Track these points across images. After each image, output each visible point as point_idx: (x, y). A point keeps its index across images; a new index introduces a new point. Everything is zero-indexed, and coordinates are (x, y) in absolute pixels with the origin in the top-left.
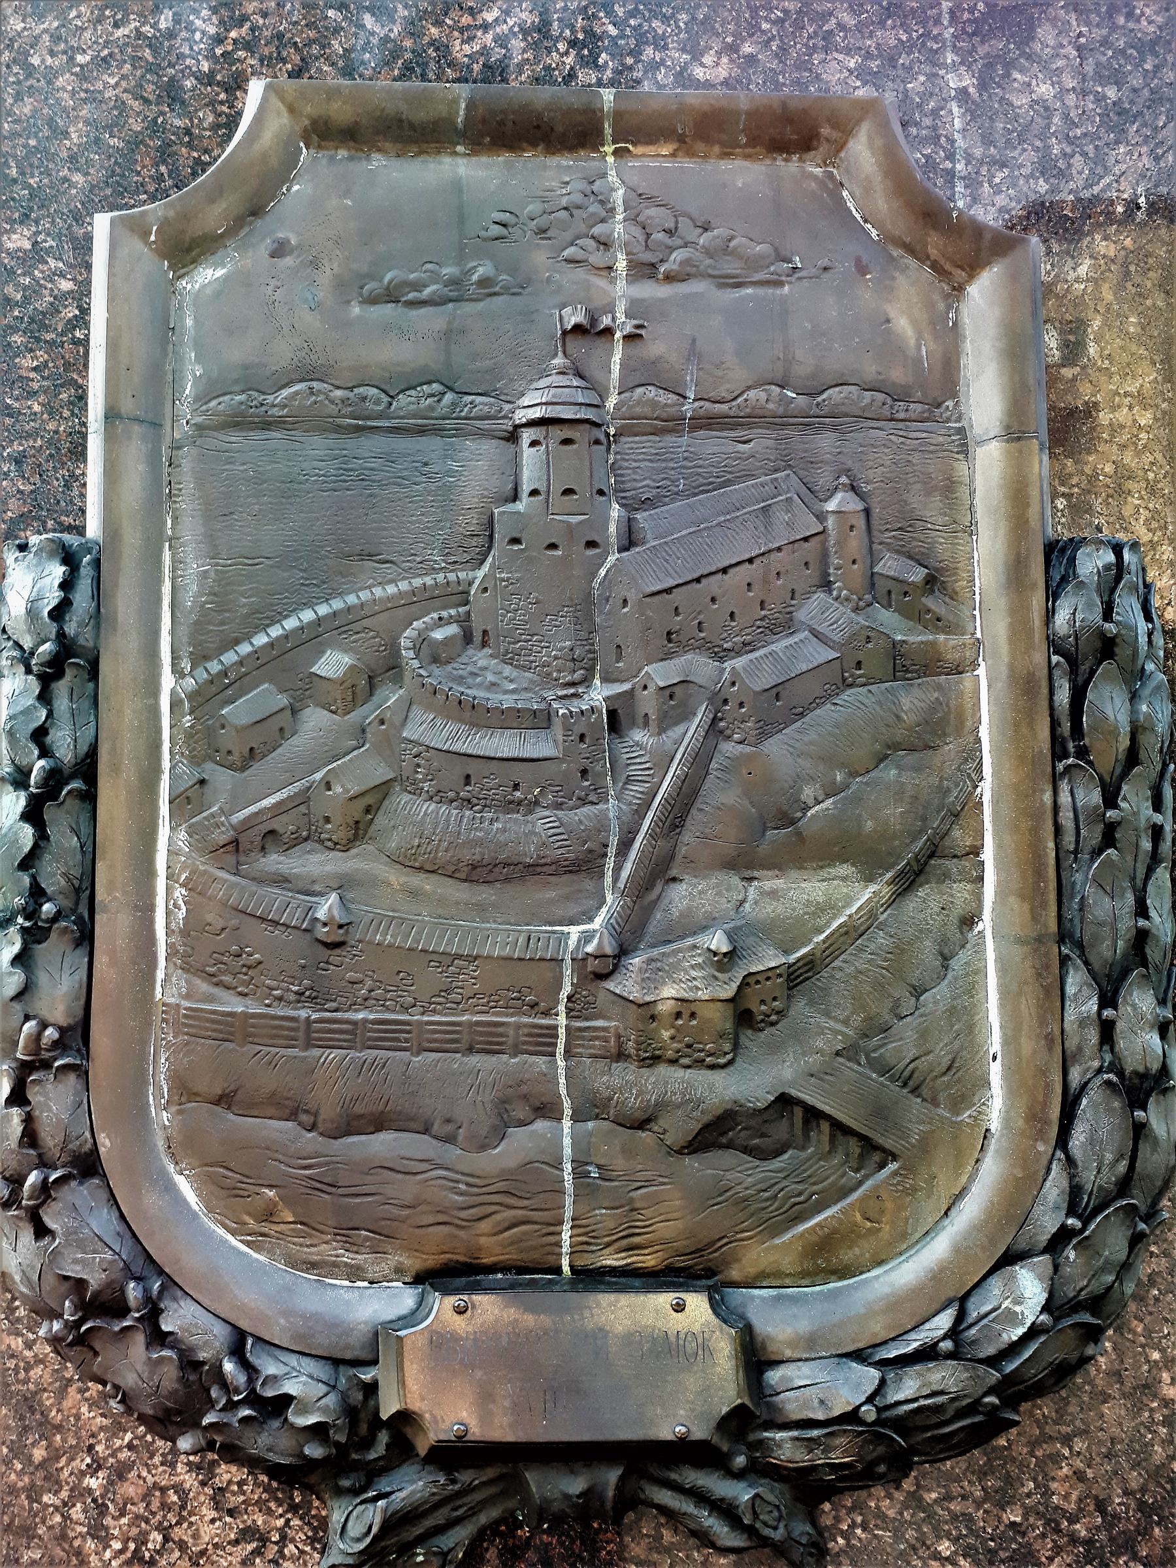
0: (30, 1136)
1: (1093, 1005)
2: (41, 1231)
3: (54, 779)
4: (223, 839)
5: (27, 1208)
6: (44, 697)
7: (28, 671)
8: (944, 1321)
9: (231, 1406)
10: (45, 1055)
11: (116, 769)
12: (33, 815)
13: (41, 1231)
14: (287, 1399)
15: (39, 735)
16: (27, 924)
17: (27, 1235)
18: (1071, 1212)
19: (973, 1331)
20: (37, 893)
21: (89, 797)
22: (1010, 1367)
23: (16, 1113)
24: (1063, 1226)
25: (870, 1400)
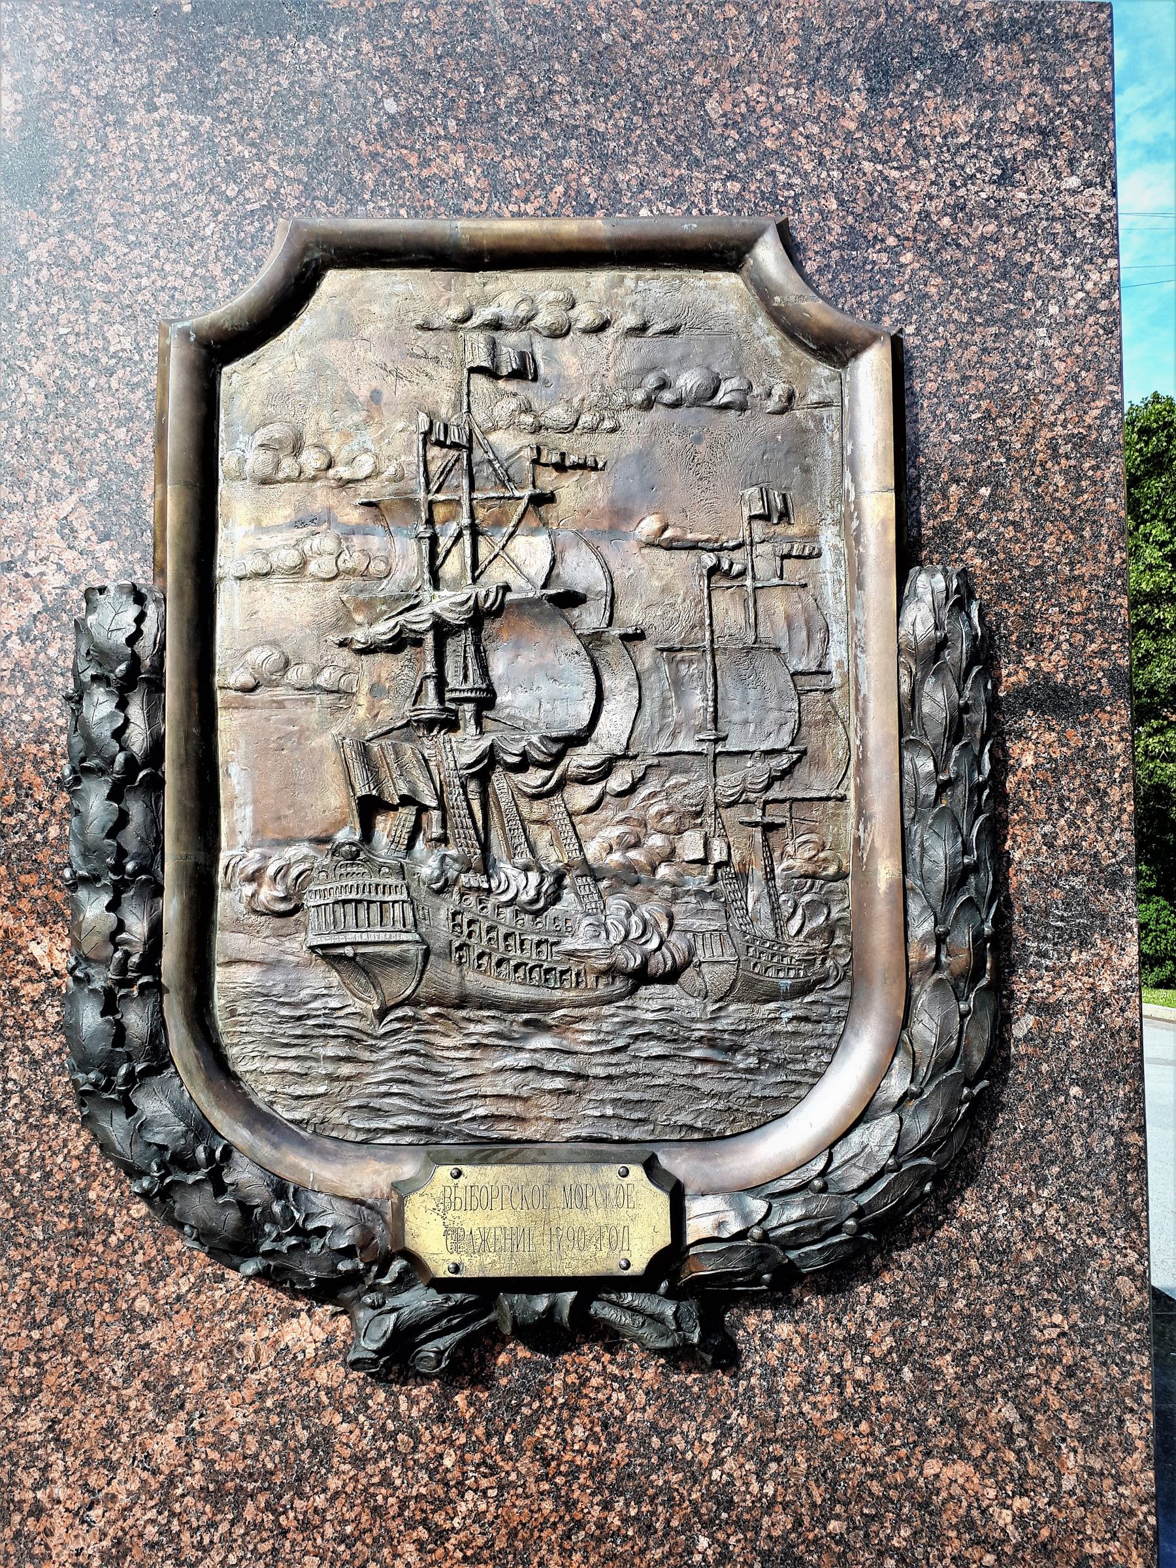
6: (122, 705)
12: (115, 795)
22: (865, 1198)
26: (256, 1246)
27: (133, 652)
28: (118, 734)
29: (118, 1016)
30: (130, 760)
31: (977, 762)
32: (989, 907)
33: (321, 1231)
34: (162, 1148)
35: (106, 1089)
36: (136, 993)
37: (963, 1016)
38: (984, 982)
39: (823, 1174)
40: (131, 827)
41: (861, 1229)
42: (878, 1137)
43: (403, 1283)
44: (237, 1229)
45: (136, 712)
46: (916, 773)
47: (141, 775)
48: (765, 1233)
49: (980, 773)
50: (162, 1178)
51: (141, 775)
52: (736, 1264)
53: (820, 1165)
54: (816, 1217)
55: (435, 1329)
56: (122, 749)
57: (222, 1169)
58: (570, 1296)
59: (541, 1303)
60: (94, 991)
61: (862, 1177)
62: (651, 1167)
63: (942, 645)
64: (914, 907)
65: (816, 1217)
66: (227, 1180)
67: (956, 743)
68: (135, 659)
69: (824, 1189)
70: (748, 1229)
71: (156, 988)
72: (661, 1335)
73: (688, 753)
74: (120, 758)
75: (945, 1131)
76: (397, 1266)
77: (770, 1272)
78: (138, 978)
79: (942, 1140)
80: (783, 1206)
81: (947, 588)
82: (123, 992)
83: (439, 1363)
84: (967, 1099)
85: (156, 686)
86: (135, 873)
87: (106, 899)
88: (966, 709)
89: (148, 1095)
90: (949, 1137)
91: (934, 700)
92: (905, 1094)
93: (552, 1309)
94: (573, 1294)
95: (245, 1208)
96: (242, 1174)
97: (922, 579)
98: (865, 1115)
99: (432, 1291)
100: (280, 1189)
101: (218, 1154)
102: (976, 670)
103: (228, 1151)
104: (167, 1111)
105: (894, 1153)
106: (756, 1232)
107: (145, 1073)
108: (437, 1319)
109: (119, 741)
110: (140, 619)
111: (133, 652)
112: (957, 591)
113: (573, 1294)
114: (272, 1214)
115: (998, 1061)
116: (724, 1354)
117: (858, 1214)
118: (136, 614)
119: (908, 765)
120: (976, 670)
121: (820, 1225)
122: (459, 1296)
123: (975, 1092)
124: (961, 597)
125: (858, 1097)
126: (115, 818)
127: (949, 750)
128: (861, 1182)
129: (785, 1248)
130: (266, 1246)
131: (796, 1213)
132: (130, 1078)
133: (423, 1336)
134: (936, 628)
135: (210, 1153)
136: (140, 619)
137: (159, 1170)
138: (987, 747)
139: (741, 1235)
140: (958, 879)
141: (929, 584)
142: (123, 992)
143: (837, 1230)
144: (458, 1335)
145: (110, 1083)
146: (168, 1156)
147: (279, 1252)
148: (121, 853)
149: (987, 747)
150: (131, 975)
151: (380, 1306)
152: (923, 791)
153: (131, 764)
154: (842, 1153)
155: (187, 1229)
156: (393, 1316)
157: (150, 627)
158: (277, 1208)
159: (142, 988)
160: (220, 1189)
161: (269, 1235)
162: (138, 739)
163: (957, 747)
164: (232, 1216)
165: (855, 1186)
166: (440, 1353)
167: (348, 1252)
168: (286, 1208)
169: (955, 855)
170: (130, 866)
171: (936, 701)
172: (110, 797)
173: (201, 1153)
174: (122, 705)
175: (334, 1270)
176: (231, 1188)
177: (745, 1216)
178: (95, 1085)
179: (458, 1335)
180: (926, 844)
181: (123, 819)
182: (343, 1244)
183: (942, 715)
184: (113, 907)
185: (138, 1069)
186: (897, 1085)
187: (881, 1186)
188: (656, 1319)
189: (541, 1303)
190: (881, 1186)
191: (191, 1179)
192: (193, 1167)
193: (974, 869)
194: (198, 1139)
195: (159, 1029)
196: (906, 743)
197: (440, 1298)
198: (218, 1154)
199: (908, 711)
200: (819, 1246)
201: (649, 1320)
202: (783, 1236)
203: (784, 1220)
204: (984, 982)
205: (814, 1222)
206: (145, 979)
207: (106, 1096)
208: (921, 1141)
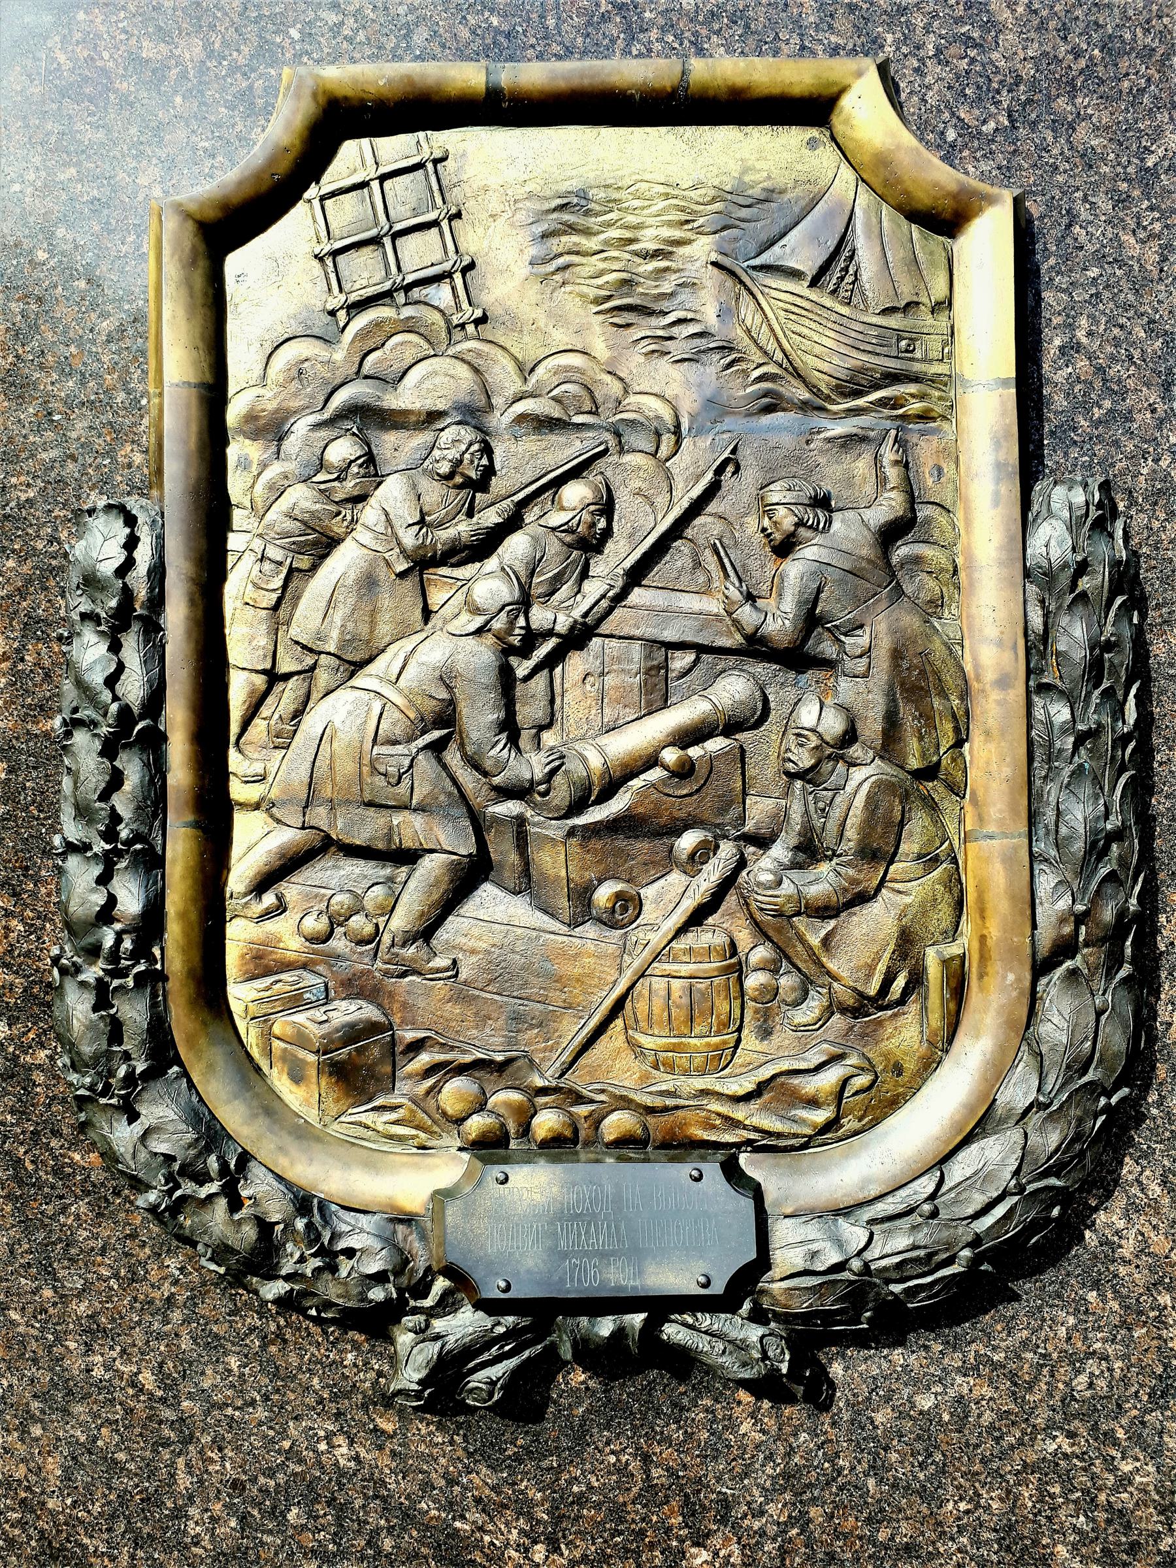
6: (115, 647)
12: (109, 750)
26: (277, 1266)
27: (125, 584)
28: (111, 681)
29: (113, 1011)
30: (125, 711)
31: (1118, 713)
32: (1135, 881)
33: (350, 1253)
34: (169, 1159)
35: (103, 1094)
36: (131, 984)
37: (1099, 1013)
38: (1122, 973)
39: (932, 1197)
40: (127, 787)
41: (975, 1261)
42: (995, 1154)
43: (447, 1305)
44: (253, 1250)
45: (132, 652)
46: (1049, 724)
48: (866, 1265)
49: (1124, 722)
50: (170, 1193)
52: (829, 1304)
53: (927, 1185)
55: (485, 1357)
56: (115, 698)
58: (637, 1319)
59: (605, 1327)
60: (83, 984)
61: (979, 1200)
62: (732, 1172)
63: (1082, 568)
64: (1046, 882)
65: (925, 1247)
66: (244, 1193)
67: (1096, 687)
68: (127, 594)
69: (934, 1214)
70: (847, 1261)
71: (153, 980)
72: (744, 1365)
74: (114, 708)
75: (1078, 1147)
76: (441, 1284)
77: (867, 1310)
78: (133, 966)
79: (1072, 1158)
80: (888, 1233)
81: (1087, 503)
82: (116, 983)
83: (491, 1394)
84: (1102, 1112)
85: (152, 628)
86: (129, 843)
87: (97, 870)
88: (1109, 646)
90: (1082, 1153)
91: (1070, 636)
92: (1031, 1106)
93: (620, 1333)
94: (643, 1316)
95: (264, 1227)
96: (258, 1186)
97: (1059, 493)
98: (981, 1123)
99: (480, 1314)
100: (303, 1202)
101: (232, 1166)
102: (1119, 600)
103: (245, 1158)
104: (173, 1116)
105: (1017, 1173)
106: (856, 1264)
107: (148, 1076)
108: (487, 1346)
109: (113, 691)
110: (131, 543)
111: (125, 584)
112: (1100, 506)
113: (643, 1316)
114: (294, 1231)
115: (1139, 1062)
116: (818, 1393)
117: (976, 1242)
118: (122, 540)
119: (1039, 713)
120: (1119, 600)
121: (930, 1256)
122: (510, 1320)
123: (1114, 1100)
124: (1102, 518)
125: (971, 1108)
126: (107, 778)
127: (1089, 694)
128: (979, 1207)
129: (888, 1281)
130: (287, 1268)
131: (901, 1242)
133: (471, 1365)
134: (1074, 549)
135: (224, 1165)
136: (131, 543)
138: (1133, 691)
139: (839, 1267)
140: (1097, 849)
141: (1065, 498)
142: (116, 983)
143: (950, 1261)
144: (513, 1362)
145: (107, 1088)
146: (176, 1167)
147: (303, 1276)
148: (115, 818)
149: (1133, 691)
150: (125, 963)
151: (423, 1331)
152: (1058, 744)
153: (126, 716)
154: (958, 1171)
155: (200, 1247)
156: (439, 1344)
157: (144, 555)
158: (300, 1224)
159: (137, 977)
160: (235, 1204)
162: (133, 688)
163: (1097, 693)
164: (250, 1232)
165: (970, 1211)
166: (493, 1383)
167: (380, 1278)
168: (309, 1226)
170: (124, 834)
171: (1074, 635)
172: (102, 754)
173: (213, 1163)
174: (115, 647)
175: (363, 1298)
176: (248, 1203)
177: (839, 1243)
178: (91, 1088)
179: (513, 1362)
180: (1062, 807)
181: (116, 781)
183: (1079, 654)
184: (104, 880)
186: (1018, 1092)
187: (1000, 1211)
188: (740, 1346)
189: (605, 1327)
190: (1000, 1211)
191: (203, 1192)
192: (202, 1178)
193: (1117, 835)
194: (208, 1150)
196: (1037, 688)
197: (488, 1322)
198: (232, 1166)
199: (1037, 646)
200: (929, 1279)
201: (730, 1347)
202: (885, 1269)
203: (888, 1250)
204: (1122, 973)
205: (922, 1253)
206: (141, 967)
207: (103, 1101)
208: (1049, 1159)
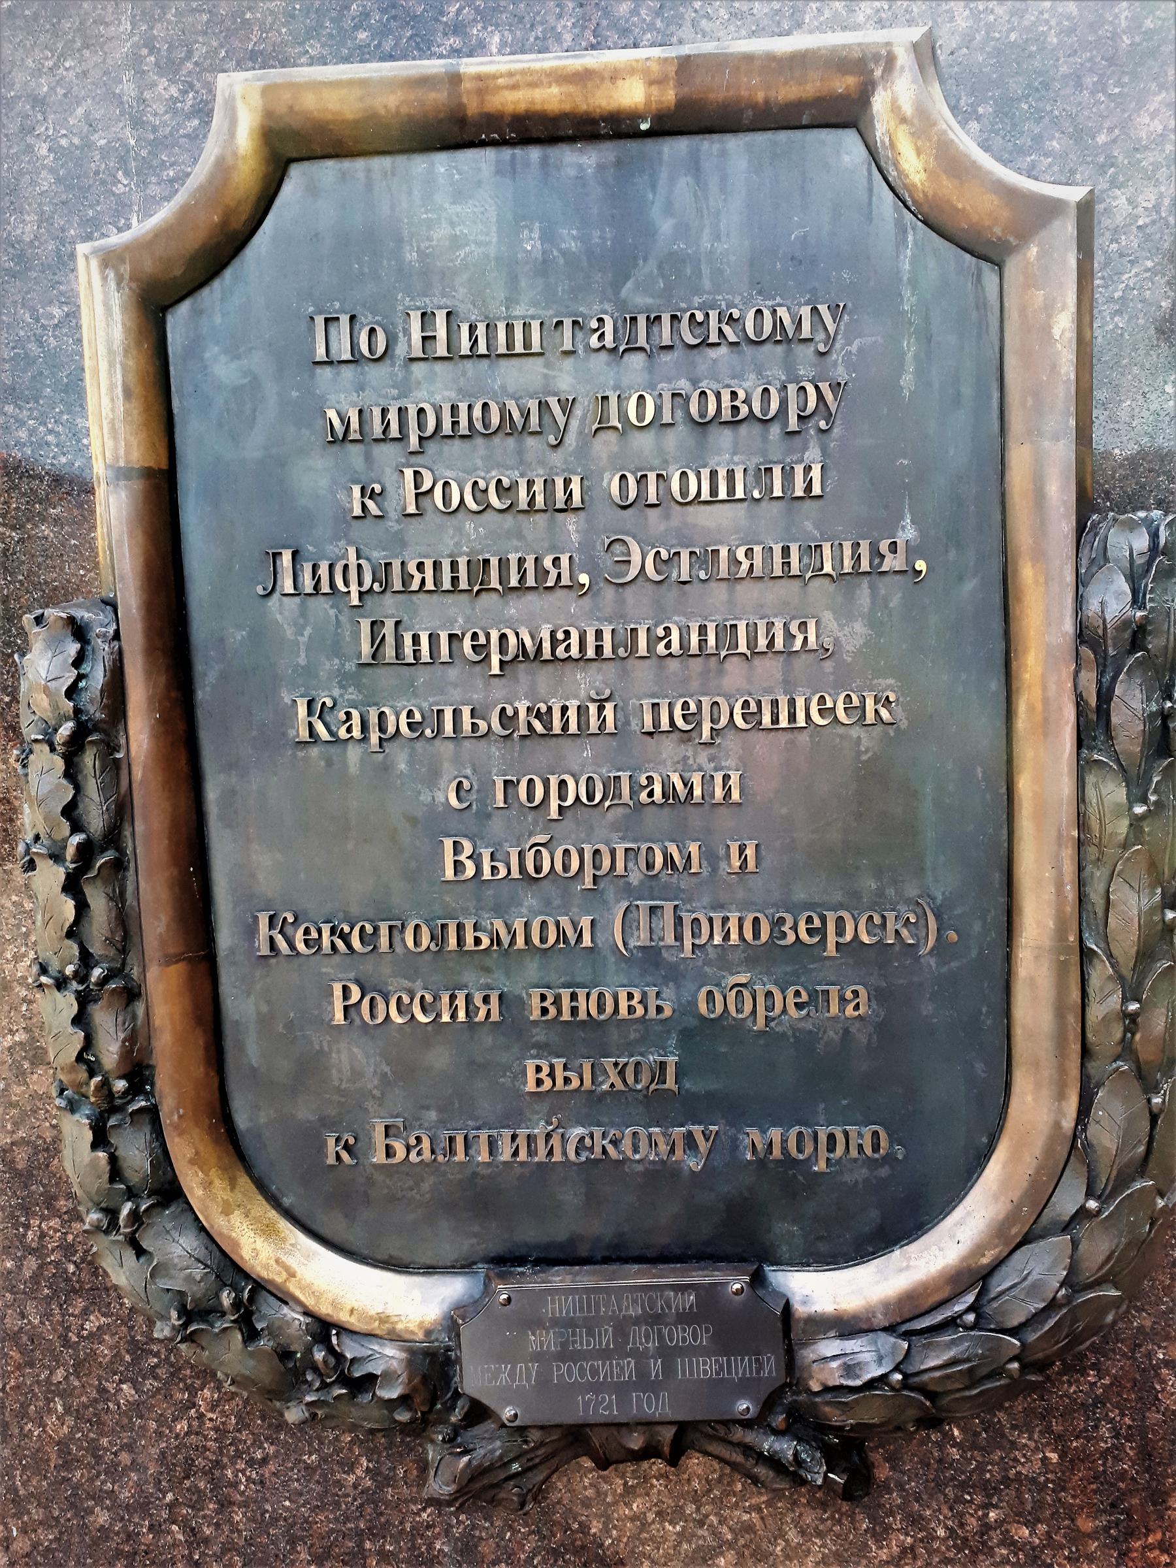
0: (116, 1171)
1: (1115, 1000)
2: (140, 1252)
3: (86, 852)
4: (879, 102)
5: (125, 1235)
6: (71, 773)
7: (53, 750)
8: (970, 1298)
9: (325, 1386)
10: (118, 1102)
11: (1039, 555)
12: (72, 886)
13: (140, 1252)
14: (371, 1378)
15: (69, 811)
16: (81, 988)
17: (129, 1254)
18: (1089, 1194)
19: (995, 1305)
20: (86, 960)
21: (119, 865)
22: (1032, 1337)
23: (102, 1155)
24: (1083, 1207)
25: (897, 1369)
47: (1138, 1185)
51: (1138, 1185)
54: (968, 1360)
57: (252, 1313)
73: (1002, 340)
89: (157, 1235)
91: (1128, 707)
119: (1091, 793)
132: (135, 1216)
137: (179, 1318)
161: (310, 1384)
169: (1152, 910)
170: (97, 973)
182: (393, 1393)
185: (143, 1208)
195: (162, 1159)
208: (1101, 1268)
